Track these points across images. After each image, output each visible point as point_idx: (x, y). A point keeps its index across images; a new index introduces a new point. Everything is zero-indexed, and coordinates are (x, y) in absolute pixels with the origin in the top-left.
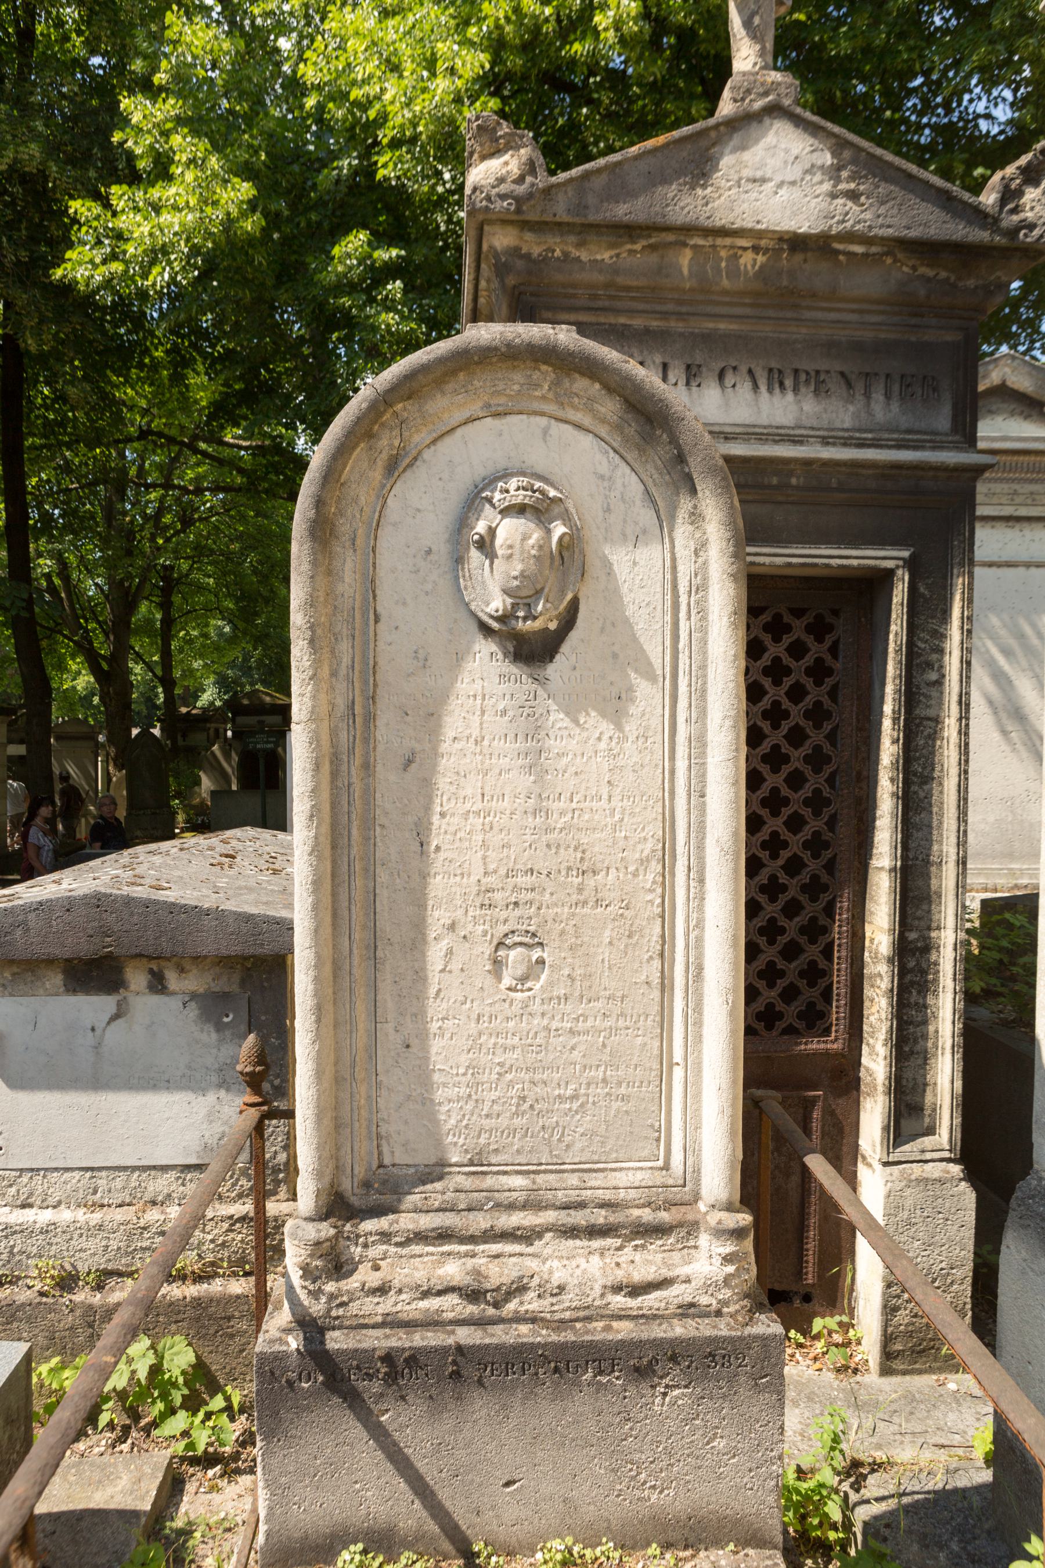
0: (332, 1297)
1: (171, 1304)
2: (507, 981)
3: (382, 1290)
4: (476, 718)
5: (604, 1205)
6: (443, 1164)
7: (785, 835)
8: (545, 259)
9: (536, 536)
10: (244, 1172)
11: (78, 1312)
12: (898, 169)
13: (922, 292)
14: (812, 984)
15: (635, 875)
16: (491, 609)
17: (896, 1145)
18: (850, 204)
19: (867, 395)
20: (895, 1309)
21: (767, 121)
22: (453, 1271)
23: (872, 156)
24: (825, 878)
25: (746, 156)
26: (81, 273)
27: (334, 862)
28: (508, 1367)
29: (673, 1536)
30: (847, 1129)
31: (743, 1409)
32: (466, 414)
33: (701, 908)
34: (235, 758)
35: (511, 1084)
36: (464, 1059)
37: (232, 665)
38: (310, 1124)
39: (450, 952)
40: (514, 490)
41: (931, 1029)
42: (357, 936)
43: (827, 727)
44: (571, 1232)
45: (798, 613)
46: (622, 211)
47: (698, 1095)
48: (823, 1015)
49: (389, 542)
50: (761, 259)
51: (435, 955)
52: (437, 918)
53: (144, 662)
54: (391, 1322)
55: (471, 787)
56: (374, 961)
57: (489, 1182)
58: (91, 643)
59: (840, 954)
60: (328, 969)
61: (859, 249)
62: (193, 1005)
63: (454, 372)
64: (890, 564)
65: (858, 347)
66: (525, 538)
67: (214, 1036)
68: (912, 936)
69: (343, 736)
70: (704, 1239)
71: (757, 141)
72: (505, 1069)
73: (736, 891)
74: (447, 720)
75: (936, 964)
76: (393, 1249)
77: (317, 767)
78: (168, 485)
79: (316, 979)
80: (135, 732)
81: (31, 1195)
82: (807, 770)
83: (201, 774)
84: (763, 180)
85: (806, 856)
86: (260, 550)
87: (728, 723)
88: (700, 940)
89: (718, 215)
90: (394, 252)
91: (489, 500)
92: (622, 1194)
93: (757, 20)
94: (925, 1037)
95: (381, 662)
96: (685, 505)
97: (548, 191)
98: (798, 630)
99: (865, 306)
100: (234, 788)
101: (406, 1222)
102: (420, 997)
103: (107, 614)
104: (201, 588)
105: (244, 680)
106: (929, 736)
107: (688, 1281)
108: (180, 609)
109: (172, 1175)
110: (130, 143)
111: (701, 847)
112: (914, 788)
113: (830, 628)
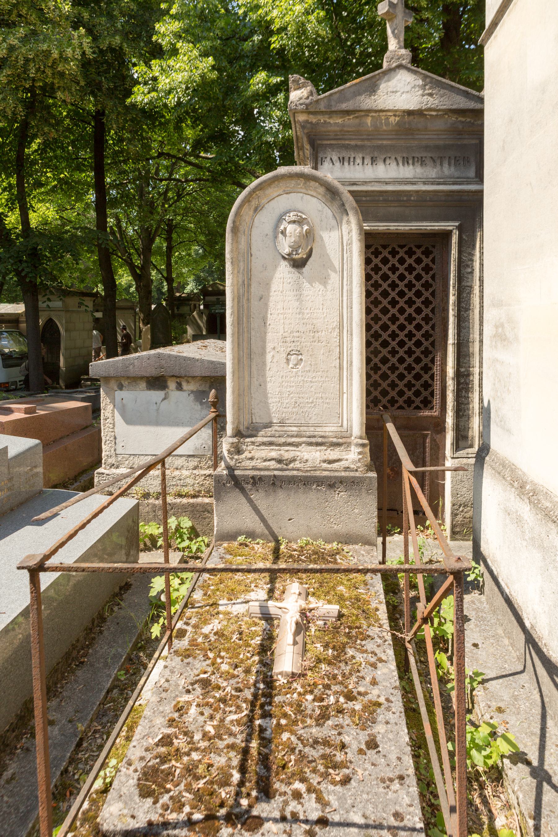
0: (237, 460)
1: (183, 505)
2: (291, 365)
3: (252, 459)
4: (281, 285)
5: (321, 437)
6: (271, 423)
7: (414, 332)
8: (317, 124)
9: (299, 230)
10: (210, 459)
11: (150, 506)
12: (448, 84)
13: (461, 127)
14: (426, 390)
15: (331, 333)
16: (285, 252)
17: (457, 451)
18: (429, 98)
19: (441, 165)
20: (456, 515)
21: (397, 70)
22: (274, 454)
23: (438, 80)
24: (431, 348)
25: (390, 84)
26: (139, 98)
27: (238, 329)
28: (290, 482)
29: (342, 540)
30: (441, 447)
31: (364, 500)
32: (278, 194)
33: (351, 343)
34: (205, 318)
35: (292, 398)
36: (278, 390)
37: (203, 270)
38: (231, 407)
39: (273, 356)
40: (292, 216)
41: (471, 406)
42: (245, 351)
43: (431, 290)
44: (310, 444)
45: (419, 247)
46: (344, 106)
47: (351, 403)
48: (430, 402)
49: (254, 232)
50: (397, 119)
51: (269, 357)
52: (269, 346)
53: (157, 269)
54: (254, 468)
55: (280, 306)
56: (250, 358)
57: (285, 429)
58: (131, 260)
59: (437, 378)
60: (236, 361)
61: (434, 113)
62: (192, 395)
63: (274, 182)
64: (451, 228)
65: (437, 148)
66: (295, 230)
67: (199, 407)
68: (462, 370)
69: (241, 290)
70: (353, 448)
71: (394, 78)
72: (290, 393)
73: (362, 338)
74: (272, 285)
75: (473, 381)
76: (255, 447)
77: (233, 300)
78: (169, 179)
79: (233, 363)
80: (153, 307)
81: (133, 464)
82: (423, 307)
83: (187, 327)
84: (396, 92)
85: (423, 340)
86: (218, 210)
87: (358, 285)
88: (351, 353)
89: (379, 105)
90: (279, 79)
91: (285, 219)
92: (327, 434)
93: (396, 31)
94: (468, 409)
95: (253, 268)
96: (345, 219)
97: (317, 101)
98: (419, 253)
99: (440, 133)
100: (204, 333)
101: (259, 439)
102: (264, 370)
103: (139, 244)
104: (187, 230)
105: (209, 278)
106: (468, 293)
107: (347, 460)
108: (176, 241)
109: (184, 458)
110: (160, 40)
111: (351, 324)
112: (462, 313)
113: (431, 252)
